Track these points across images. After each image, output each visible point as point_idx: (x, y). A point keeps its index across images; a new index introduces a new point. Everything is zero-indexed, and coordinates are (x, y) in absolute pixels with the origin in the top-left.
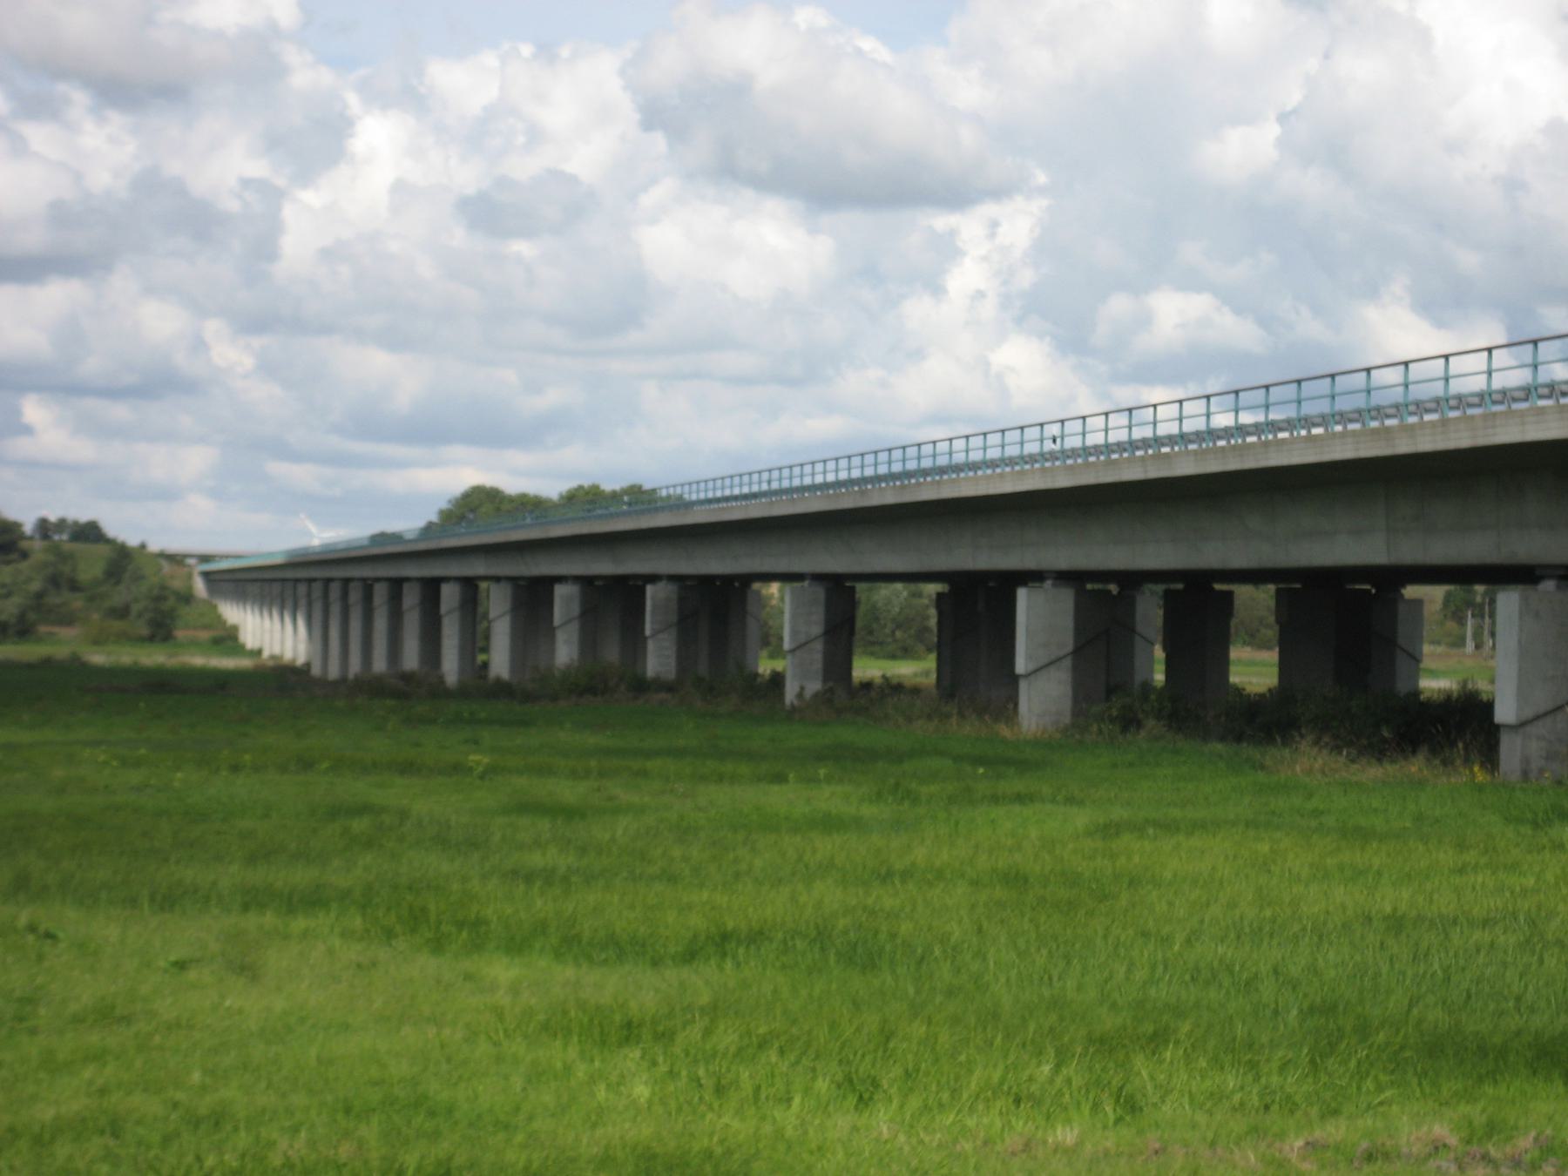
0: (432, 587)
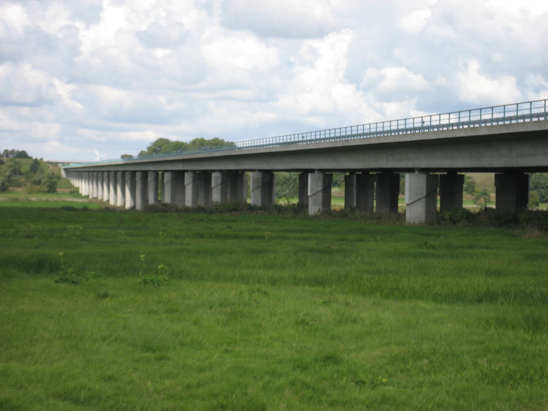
0: (145, 174)
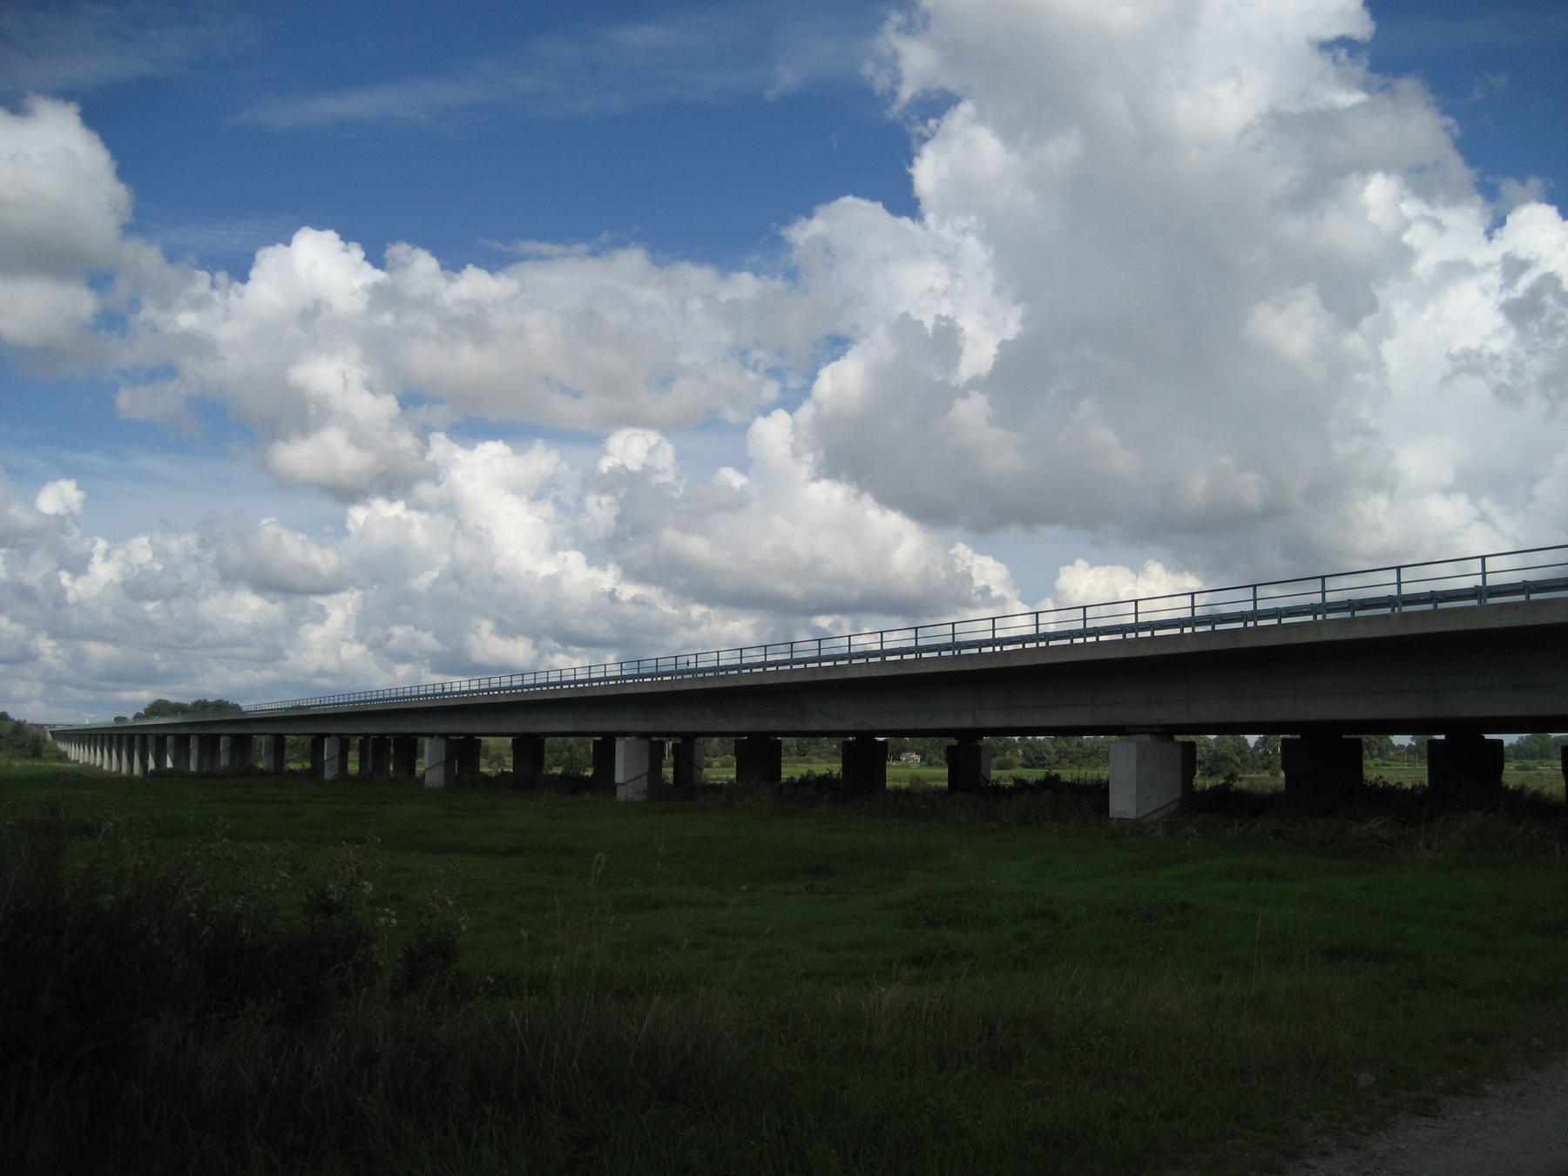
0: (144, 737)
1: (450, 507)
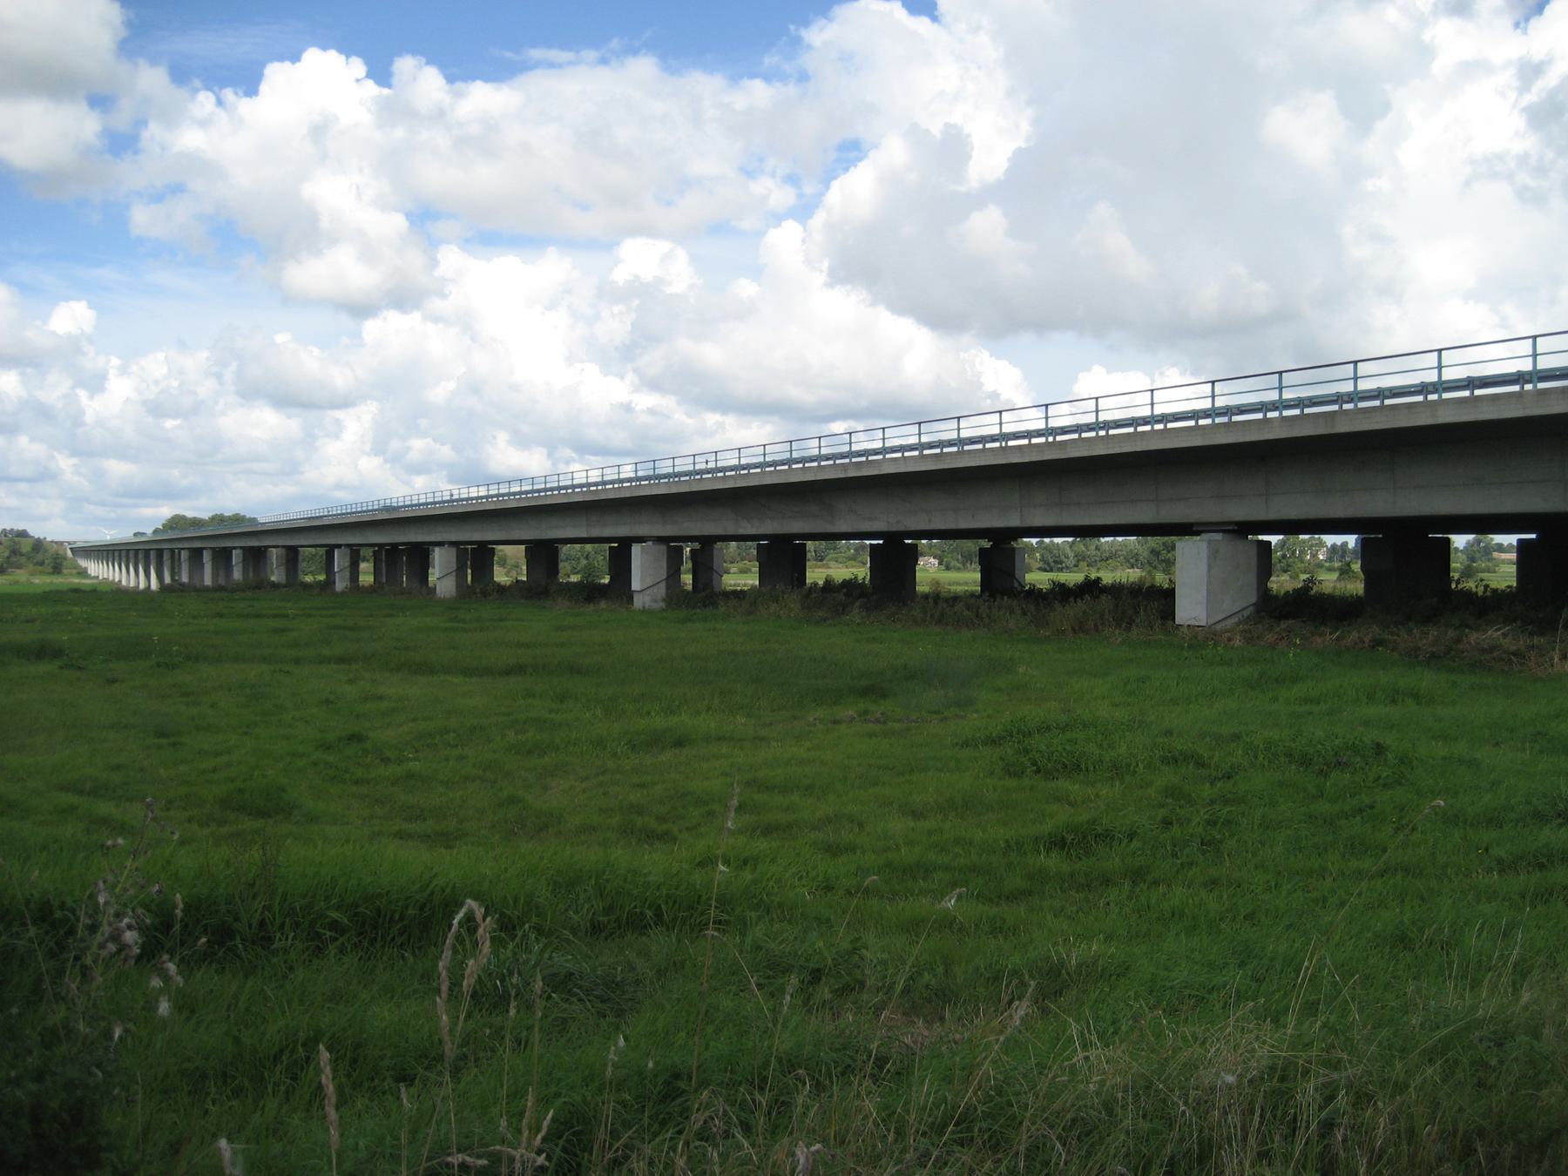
0: (160, 552)
1: (465, 323)
